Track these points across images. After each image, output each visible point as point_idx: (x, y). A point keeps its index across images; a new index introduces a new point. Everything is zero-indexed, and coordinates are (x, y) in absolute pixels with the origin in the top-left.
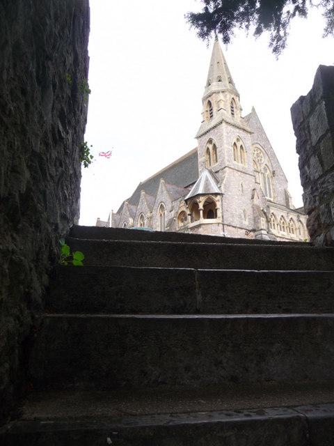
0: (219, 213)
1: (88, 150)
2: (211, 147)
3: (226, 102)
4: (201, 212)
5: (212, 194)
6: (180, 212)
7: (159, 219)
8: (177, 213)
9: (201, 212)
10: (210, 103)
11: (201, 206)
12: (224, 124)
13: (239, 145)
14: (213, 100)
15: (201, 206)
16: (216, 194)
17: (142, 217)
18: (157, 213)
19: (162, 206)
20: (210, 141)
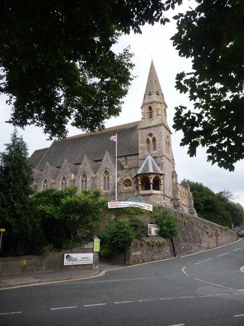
0: (162, 187)
1: (15, 126)
2: (151, 139)
3: (162, 110)
4: (151, 185)
5: (159, 174)
6: (125, 179)
7: (103, 180)
8: (122, 179)
9: (151, 185)
10: (150, 108)
11: (151, 181)
12: (163, 126)
13: (151, 139)
14: (154, 107)
15: (151, 181)
16: (161, 175)
17: (84, 175)
18: (101, 175)
19: (106, 172)
20: (151, 135)
